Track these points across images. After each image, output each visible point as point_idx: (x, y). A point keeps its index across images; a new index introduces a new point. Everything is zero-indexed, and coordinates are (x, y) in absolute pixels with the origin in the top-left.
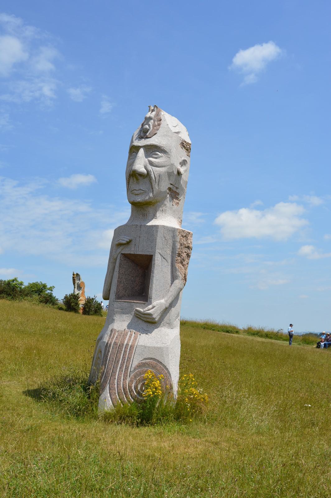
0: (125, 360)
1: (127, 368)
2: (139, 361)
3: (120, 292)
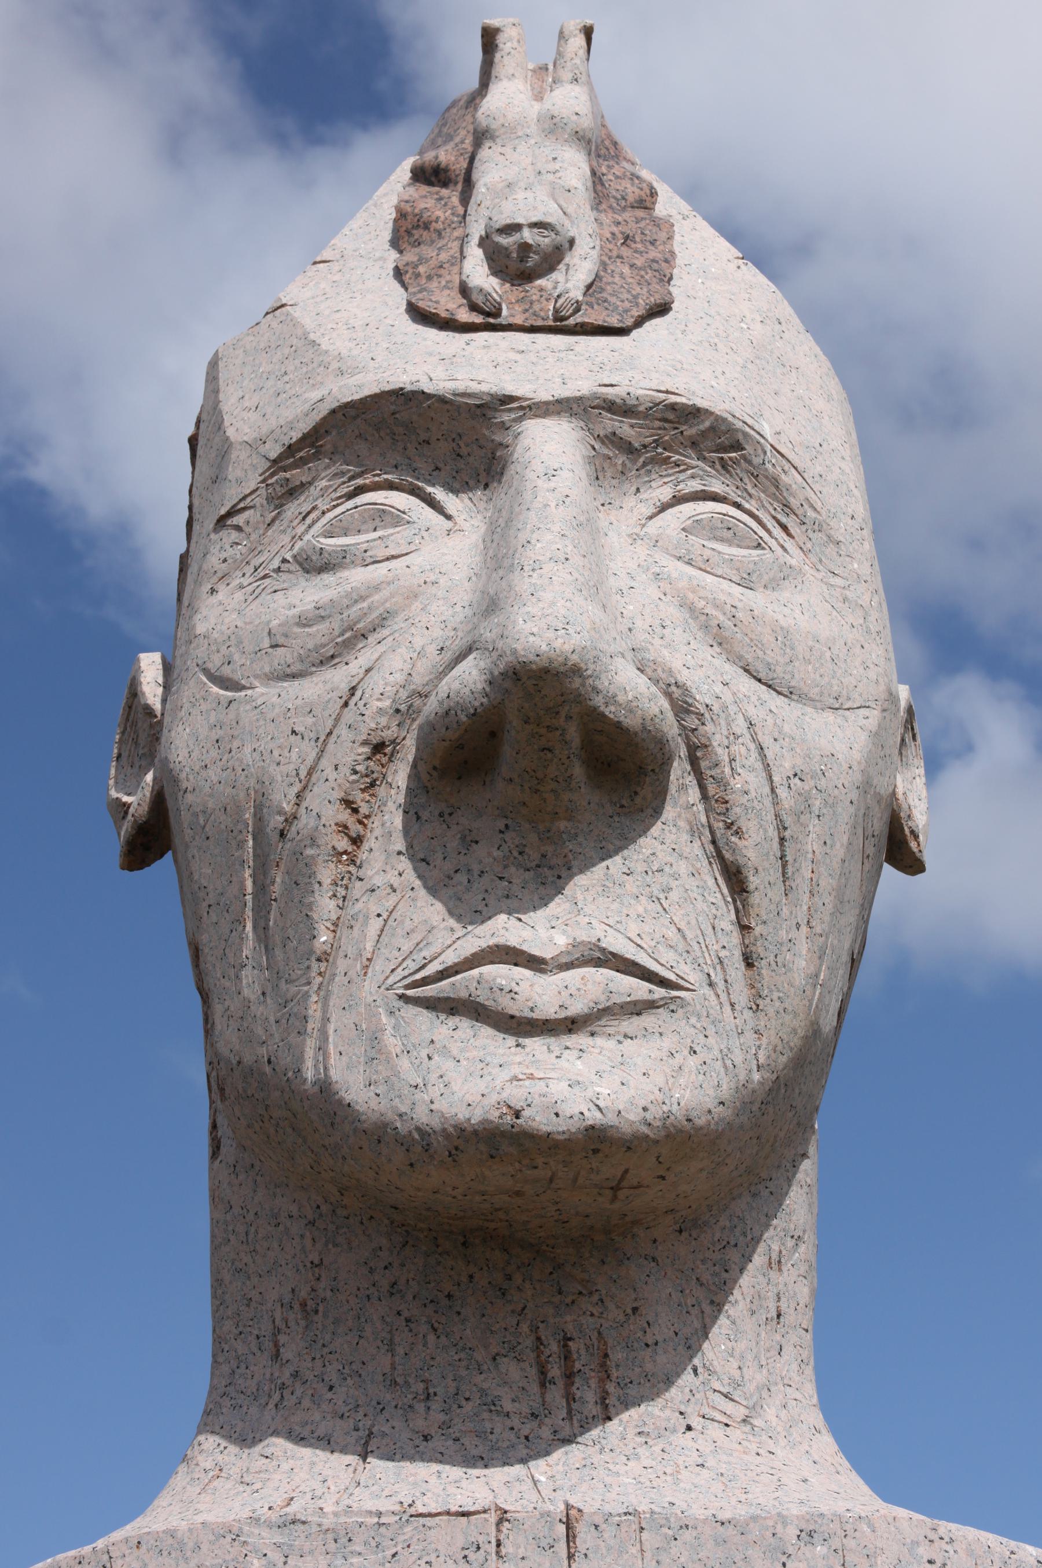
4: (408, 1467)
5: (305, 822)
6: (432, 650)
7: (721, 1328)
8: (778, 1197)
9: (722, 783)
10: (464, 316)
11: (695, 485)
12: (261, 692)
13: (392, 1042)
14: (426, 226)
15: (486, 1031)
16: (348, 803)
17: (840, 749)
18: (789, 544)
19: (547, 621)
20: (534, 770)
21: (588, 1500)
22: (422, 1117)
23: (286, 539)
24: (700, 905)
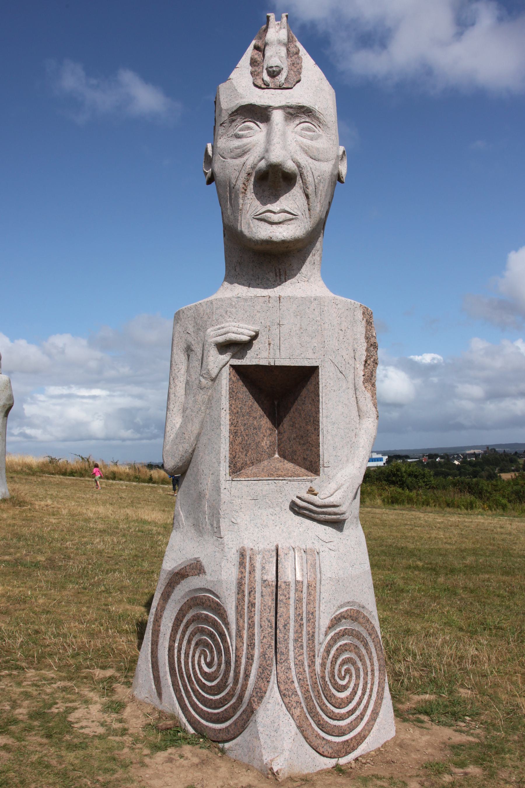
1: (312, 638)
2: (330, 615)
3: (237, 456)
5: (237, 187)
6: (257, 157)
7: (304, 267)
8: (315, 245)
9: (305, 180)
10: (263, 86)
11: (303, 120)
12: (229, 160)
13: (252, 225)
14: (256, 62)
15: (266, 224)
16: (244, 184)
17: (327, 169)
18: (320, 130)
19: (277, 156)
20: (274, 180)
21: (282, 294)
22: (256, 238)
23: (232, 130)
24: (301, 201)
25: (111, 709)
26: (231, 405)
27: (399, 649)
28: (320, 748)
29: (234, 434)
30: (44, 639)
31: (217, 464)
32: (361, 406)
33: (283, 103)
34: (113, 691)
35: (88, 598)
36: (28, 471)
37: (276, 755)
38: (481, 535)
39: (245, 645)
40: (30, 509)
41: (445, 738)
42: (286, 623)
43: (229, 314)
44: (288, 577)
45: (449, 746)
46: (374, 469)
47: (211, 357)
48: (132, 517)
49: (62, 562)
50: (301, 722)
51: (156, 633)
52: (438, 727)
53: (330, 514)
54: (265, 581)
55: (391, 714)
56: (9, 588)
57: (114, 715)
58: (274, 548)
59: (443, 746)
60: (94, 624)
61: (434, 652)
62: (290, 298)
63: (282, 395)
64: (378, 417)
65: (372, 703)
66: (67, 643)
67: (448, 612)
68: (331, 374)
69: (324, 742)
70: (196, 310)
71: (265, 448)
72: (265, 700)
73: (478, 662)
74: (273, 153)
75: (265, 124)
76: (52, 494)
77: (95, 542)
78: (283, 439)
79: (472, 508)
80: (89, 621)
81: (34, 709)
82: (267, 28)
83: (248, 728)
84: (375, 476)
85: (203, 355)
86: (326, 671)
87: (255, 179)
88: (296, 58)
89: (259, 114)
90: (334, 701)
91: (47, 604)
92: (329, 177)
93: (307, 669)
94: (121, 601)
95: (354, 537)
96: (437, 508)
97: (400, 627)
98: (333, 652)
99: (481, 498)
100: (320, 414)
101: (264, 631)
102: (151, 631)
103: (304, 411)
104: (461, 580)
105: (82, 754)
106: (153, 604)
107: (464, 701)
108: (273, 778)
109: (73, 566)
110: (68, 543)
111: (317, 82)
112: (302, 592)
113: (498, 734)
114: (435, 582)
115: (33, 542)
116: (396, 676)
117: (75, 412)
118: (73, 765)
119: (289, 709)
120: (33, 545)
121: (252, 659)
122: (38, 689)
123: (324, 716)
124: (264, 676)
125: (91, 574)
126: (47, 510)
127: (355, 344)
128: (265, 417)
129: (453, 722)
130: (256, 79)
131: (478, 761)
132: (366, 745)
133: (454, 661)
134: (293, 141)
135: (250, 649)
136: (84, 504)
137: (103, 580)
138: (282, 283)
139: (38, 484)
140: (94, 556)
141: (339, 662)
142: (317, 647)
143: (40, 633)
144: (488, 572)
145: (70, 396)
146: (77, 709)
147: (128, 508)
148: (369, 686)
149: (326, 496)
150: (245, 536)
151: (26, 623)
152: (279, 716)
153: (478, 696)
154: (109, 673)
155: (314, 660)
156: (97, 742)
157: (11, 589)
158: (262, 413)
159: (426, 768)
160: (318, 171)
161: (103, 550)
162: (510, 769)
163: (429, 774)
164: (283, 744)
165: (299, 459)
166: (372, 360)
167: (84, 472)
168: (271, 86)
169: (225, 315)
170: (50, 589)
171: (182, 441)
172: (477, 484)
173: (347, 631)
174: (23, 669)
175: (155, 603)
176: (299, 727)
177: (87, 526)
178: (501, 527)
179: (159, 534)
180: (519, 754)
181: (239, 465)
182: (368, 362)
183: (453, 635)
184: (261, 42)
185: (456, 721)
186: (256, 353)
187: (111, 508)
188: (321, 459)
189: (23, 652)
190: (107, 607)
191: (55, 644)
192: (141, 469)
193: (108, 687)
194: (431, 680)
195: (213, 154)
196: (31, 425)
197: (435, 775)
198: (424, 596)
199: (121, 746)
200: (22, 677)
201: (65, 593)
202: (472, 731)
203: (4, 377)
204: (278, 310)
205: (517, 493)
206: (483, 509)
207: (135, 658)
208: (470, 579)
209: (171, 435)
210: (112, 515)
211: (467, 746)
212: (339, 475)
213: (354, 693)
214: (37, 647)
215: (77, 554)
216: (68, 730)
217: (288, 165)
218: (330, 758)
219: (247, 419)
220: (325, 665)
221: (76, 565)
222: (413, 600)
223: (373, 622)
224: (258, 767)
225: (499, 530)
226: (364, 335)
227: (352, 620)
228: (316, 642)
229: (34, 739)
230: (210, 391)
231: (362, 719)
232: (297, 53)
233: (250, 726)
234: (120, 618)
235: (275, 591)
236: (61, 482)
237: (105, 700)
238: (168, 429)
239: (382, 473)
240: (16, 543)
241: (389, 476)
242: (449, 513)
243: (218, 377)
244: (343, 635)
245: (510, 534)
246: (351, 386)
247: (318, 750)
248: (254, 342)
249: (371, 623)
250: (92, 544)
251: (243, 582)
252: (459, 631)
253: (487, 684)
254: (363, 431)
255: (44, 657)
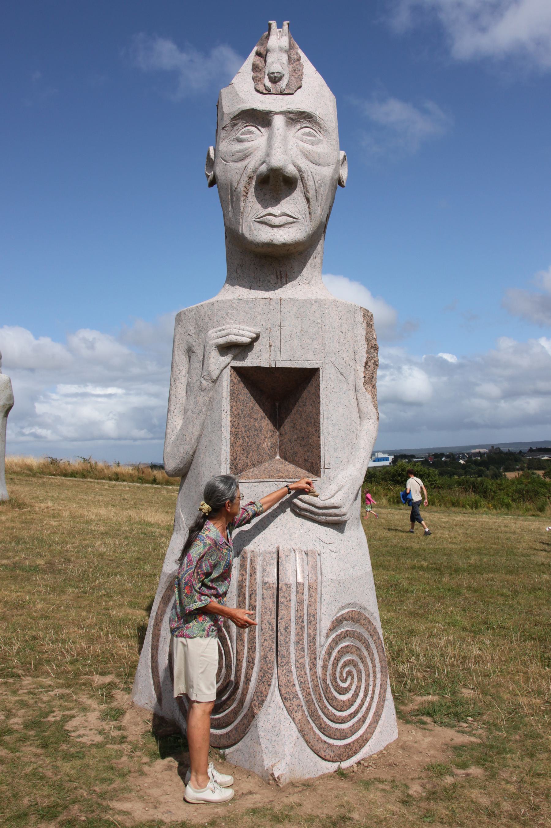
0: (303, 622)
1: (313, 640)
3: (238, 458)
4: (257, 291)
5: (238, 190)
6: (259, 160)
8: (315, 247)
9: (306, 184)
10: (265, 92)
11: (304, 125)
13: (253, 228)
14: (258, 68)
15: (267, 227)
16: (245, 187)
17: (328, 174)
18: (321, 135)
19: (278, 160)
20: (275, 184)
21: (283, 297)
22: (257, 240)
23: (234, 134)
25: (110, 716)
26: (232, 407)
27: (403, 650)
28: (322, 752)
29: (234, 436)
30: (42, 645)
31: (217, 466)
32: (362, 408)
33: (284, 109)
34: (112, 698)
35: (88, 602)
36: (28, 472)
37: (277, 760)
38: (485, 534)
39: (246, 648)
40: (29, 511)
41: (448, 740)
42: (287, 625)
43: (230, 316)
44: (289, 579)
45: (451, 747)
46: (379, 469)
47: (212, 359)
48: (135, 519)
49: (62, 565)
50: (303, 725)
51: (156, 637)
52: (440, 728)
53: (331, 515)
54: (266, 583)
55: (394, 715)
56: (6, 593)
57: (113, 723)
58: (275, 550)
59: (445, 747)
60: (94, 629)
61: (437, 652)
62: (290, 300)
63: (283, 396)
64: (378, 418)
65: (374, 705)
66: (65, 649)
67: (452, 612)
68: (332, 376)
69: (326, 746)
70: (198, 311)
71: (267, 449)
72: (266, 703)
73: (481, 662)
74: (274, 158)
75: (267, 128)
76: (53, 496)
77: (96, 545)
78: (284, 441)
79: (477, 507)
80: (88, 626)
81: (30, 718)
82: (269, 34)
83: (249, 733)
84: (381, 476)
85: (204, 357)
86: (328, 674)
87: (256, 182)
88: (297, 65)
89: (260, 119)
90: (335, 704)
91: (46, 609)
92: (330, 182)
93: (308, 672)
94: (122, 605)
95: (355, 538)
96: (442, 508)
97: (404, 628)
98: (334, 654)
99: (485, 497)
100: (321, 416)
101: (265, 634)
102: (151, 636)
103: (305, 413)
104: (465, 579)
105: (79, 764)
106: (153, 608)
107: (467, 702)
108: (274, 783)
109: (74, 570)
110: (68, 546)
111: (318, 88)
112: (303, 594)
113: (500, 734)
114: (440, 582)
115: (33, 545)
116: (399, 677)
117: (88, 412)
118: (69, 776)
119: (290, 713)
120: (32, 549)
121: (253, 663)
122: (35, 697)
123: (326, 720)
124: (265, 680)
125: (92, 578)
126: (48, 512)
127: (355, 346)
128: (267, 418)
129: (456, 723)
130: (257, 84)
131: (479, 762)
132: (368, 748)
133: (457, 661)
134: (294, 146)
135: (251, 652)
136: (85, 506)
137: (104, 584)
138: (283, 285)
139: (38, 486)
140: (95, 559)
141: (340, 664)
142: (318, 649)
143: (37, 639)
144: (492, 571)
145: (84, 395)
146: (74, 717)
147: (130, 510)
148: (371, 688)
149: (327, 497)
150: (246, 538)
151: (23, 628)
152: (280, 720)
153: (481, 696)
154: (108, 679)
155: (315, 663)
156: (94, 751)
157: (8, 594)
158: (263, 414)
159: (428, 769)
160: (319, 175)
161: (105, 552)
162: (511, 769)
163: (431, 776)
164: (284, 748)
165: (301, 460)
166: (373, 361)
167: (88, 473)
168: (272, 92)
169: (226, 317)
170: (49, 594)
171: (183, 443)
172: (482, 483)
173: (348, 633)
174: (20, 676)
175: (155, 607)
176: (300, 731)
177: (88, 529)
178: (506, 526)
179: (162, 536)
180: (521, 753)
181: (240, 466)
182: (369, 364)
183: (457, 635)
184: (262, 48)
185: (458, 721)
186: (257, 355)
187: (113, 510)
188: (322, 461)
189: (19, 659)
190: (108, 611)
191: (53, 650)
192: (145, 470)
193: (107, 693)
194: (434, 681)
195: (215, 157)
196: (42, 425)
197: (436, 777)
198: (428, 596)
199: (119, 754)
200: (17, 686)
201: (64, 597)
202: (474, 732)
203: (4, 377)
204: (279, 312)
205: (519, 491)
206: (488, 508)
207: (136, 663)
208: (474, 579)
209: (172, 437)
210: (114, 517)
211: (469, 747)
212: (340, 476)
213: (356, 695)
214: (34, 654)
215: (77, 557)
216: (65, 739)
217: (289, 169)
218: (332, 762)
219: (248, 420)
220: (327, 668)
221: (76, 569)
222: (417, 600)
223: (375, 624)
224: (259, 773)
225: (503, 529)
226: (364, 337)
227: (353, 621)
228: (318, 644)
229: (29, 750)
230: (211, 393)
231: (364, 722)
232: (299, 60)
233: (250, 730)
234: (120, 622)
235: (275, 593)
236: (63, 483)
237: (103, 707)
238: (168, 431)
239: (387, 473)
240: (15, 547)
241: (394, 476)
242: (454, 512)
243: (219, 379)
244: (345, 637)
245: (514, 533)
246: (352, 388)
247: (320, 754)
248: (255, 344)
249: (373, 624)
250: (94, 546)
251: (244, 585)
252: (463, 630)
253: (489, 684)
254: (363, 433)
255: (42, 664)
